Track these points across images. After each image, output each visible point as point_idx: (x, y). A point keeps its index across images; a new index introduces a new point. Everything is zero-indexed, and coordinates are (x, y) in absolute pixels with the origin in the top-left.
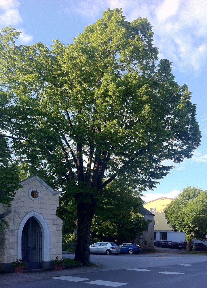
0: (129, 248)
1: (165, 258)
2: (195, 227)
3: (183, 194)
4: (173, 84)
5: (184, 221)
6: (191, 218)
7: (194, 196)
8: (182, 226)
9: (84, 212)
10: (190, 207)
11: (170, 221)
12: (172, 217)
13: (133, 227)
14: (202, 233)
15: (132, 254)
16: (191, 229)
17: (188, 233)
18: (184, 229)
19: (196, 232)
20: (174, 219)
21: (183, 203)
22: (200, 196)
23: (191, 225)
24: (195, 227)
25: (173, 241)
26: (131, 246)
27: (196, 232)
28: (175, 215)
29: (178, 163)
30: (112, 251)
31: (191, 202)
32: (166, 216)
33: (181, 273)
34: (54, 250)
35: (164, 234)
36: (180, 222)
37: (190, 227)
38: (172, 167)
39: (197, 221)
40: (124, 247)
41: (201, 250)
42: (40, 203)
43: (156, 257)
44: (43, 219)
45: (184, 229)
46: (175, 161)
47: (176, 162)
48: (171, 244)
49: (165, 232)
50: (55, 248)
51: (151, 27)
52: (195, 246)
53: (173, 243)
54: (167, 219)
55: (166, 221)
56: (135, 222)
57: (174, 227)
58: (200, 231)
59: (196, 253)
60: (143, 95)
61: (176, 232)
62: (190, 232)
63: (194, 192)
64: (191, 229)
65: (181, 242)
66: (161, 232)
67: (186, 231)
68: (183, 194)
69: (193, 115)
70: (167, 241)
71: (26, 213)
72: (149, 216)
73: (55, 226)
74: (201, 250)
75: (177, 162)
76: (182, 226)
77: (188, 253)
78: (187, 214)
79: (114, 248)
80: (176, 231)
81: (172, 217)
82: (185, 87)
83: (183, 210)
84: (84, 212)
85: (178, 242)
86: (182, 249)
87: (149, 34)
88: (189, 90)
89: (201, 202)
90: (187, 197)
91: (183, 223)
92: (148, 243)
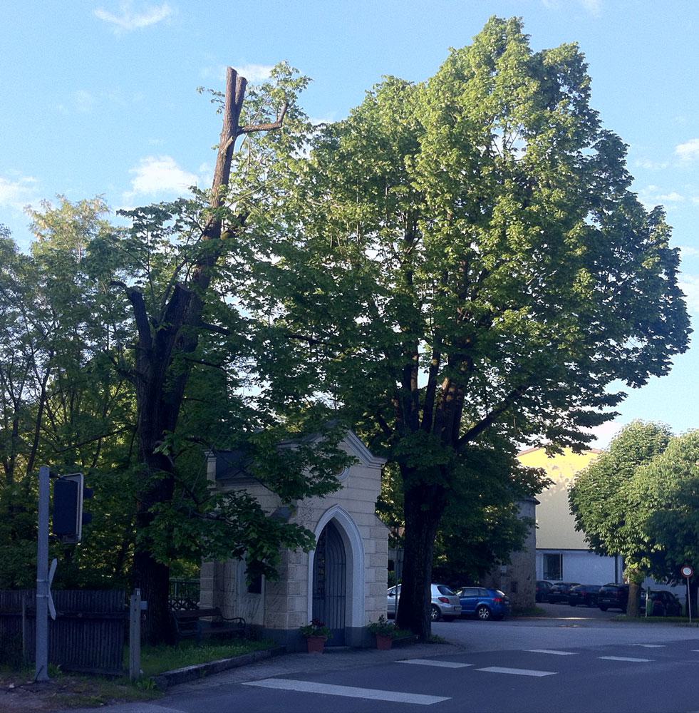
0: (478, 601)
1: (577, 630)
2: (653, 542)
3: (622, 443)
4: (631, 201)
5: (622, 523)
6: (643, 515)
7: (650, 449)
8: (618, 537)
9: (424, 508)
10: (642, 484)
11: (585, 523)
12: (590, 512)
13: (487, 538)
14: (673, 562)
15: (487, 619)
16: (642, 547)
17: (633, 560)
18: (624, 547)
19: (657, 558)
20: (596, 518)
21: (620, 469)
22: (671, 451)
23: (644, 537)
24: (653, 542)
25: (582, 584)
26: (484, 596)
27: (657, 558)
28: (601, 507)
29: (637, 388)
30: (442, 607)
31: (642, 468)
32: (575, 508)
33: (647, 660)
34: (372, 599)
35: (554, 560)
36: (614, 525)
37: (640, 541)
38: (623, 398)
39: (661, 525)
40: (464, 597)
41: (665, 614)
42: (348, 487)
43: (557, 626)
44: (352, 525)
45: (624, 547)
46: (629, 384)
47: (632, 385)
48: (577, 591)
49: (558, 552)
50: (373, 596)
51: (585, 66)
52: (653, 599)
53: (584, 587)
54: (575, 516)
55: (572, 521)
56: (493, 524)
57: (595, 540)
58: (669, 556)
59: (655, 621)
60: (576, 246)
61: (601, 556)
62: (637, 557)
63: (651, 438)
64: (642, 547)
65: (609, 588)
66: (545, 555)
67: (629, 553)
68: (622, 443)
69: (672, 273)
70: (563, 584)
71: (323, 511)
72: (525, 505)
73: (373, 542)
74: (665, 614)
75: (634, 387)
76: (618, 537)
77: (634, 621)
78: (632, 503)
79: (447, 601)
80: (602, 552)
81: (590, 512)
82: (658, 212)
83: (622, 490)
84: (424, 508)
85: (600, 587)
86: (609, 609)
87: (583, 86)
88: (668, 220)
89: (671, 473)
90: (632, 453)
91: (621, 530)
92: (520, 588)
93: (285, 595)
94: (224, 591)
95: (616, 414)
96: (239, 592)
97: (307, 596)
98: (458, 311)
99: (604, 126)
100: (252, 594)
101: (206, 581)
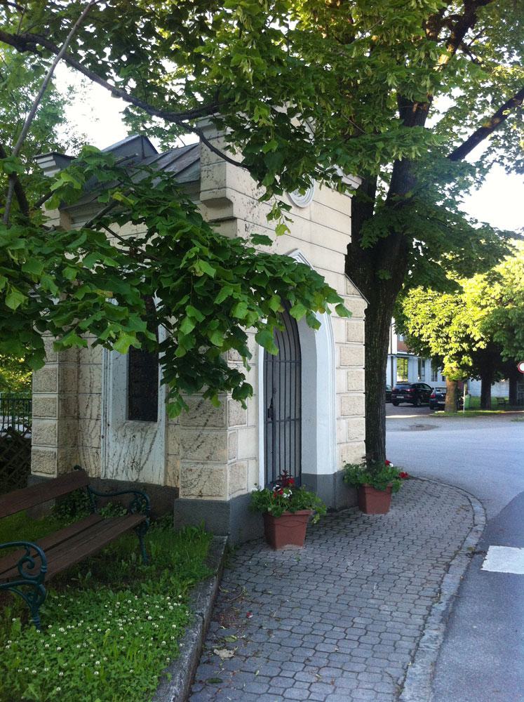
93: (223, 427)
94: (78, 418)
95: (461, 201)
96: (110, 420)
97: (256, 426)
98: (225, 46)
99: (121, 98)
100: (137, 423)
101: (45, 397)
